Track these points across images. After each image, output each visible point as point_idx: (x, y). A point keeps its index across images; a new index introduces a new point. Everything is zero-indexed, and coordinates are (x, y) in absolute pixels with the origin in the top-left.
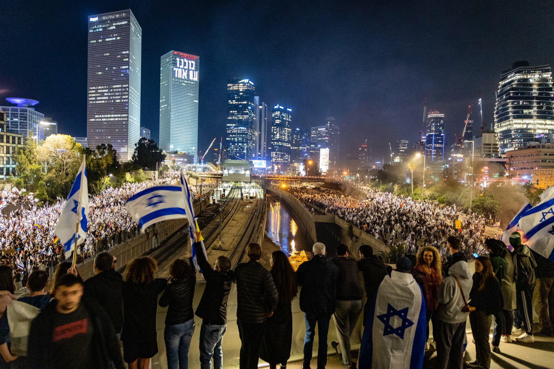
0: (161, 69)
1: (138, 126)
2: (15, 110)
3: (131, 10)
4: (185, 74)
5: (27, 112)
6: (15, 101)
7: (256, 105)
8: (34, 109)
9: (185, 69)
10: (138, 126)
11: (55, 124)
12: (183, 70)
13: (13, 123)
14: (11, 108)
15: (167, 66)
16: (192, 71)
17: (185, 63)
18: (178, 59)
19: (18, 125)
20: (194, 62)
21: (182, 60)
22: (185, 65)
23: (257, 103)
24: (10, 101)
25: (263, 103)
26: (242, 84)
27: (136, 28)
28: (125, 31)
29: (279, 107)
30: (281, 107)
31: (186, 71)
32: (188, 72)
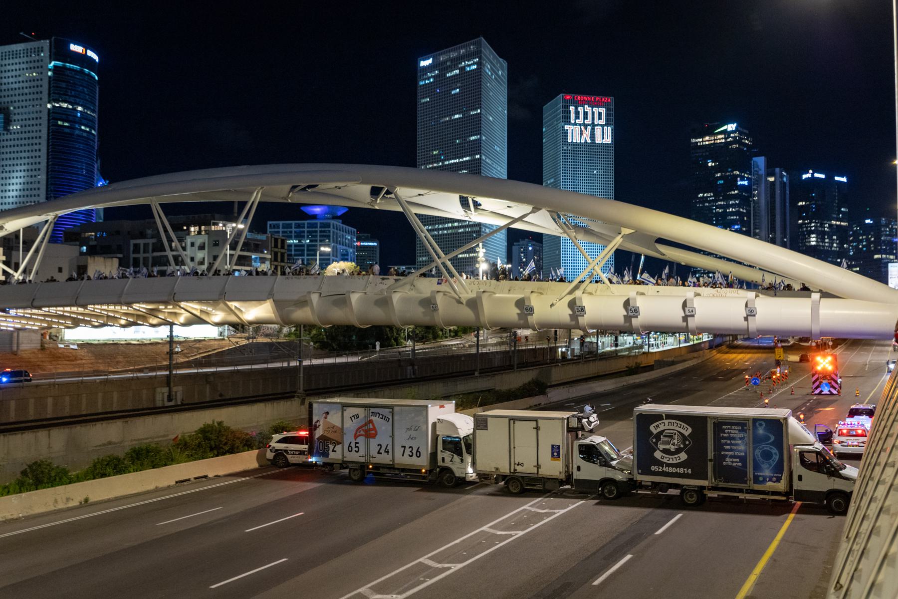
0: (544, 130)
1: (503, 240)
2: (310, 225)
3: (482, 38)
4: (587, 133)
5: (329, 227)
6: (314, 211)
7: (760, 176)
8: (341, 221)
10: (503, 240)
11: (376, 244)
13: (310, 248)
14: (321, 223)
17: (586, 114)
18: (572, 108)
19: (304, 250)
20: (603, 110)
21: (580, 109)
23: (762, 172)
24: (305, 211)
25: (777, 170)
26: (722, 136)
27: (494, 65)
28: (473, 82)
29: (813, 174)
30: (816, 175)
31: (589, 128)
32: (593, 130)
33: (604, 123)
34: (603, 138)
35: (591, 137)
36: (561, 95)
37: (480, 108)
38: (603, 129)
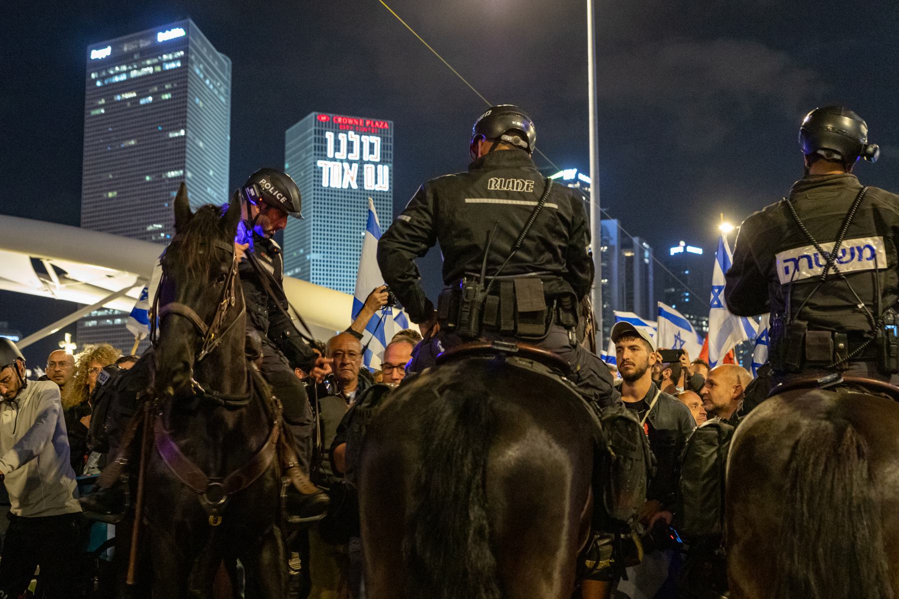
0: (287, 166)
9: (351, 162)
12: (346, 165)
15: (300, 157)
16: (373, 166)
17: (350, 144)
18: (329, 136)
20: (376, 140)
22: (350, 149)
27: (209, 64)
29: (685, 248)
30: (690, 249)
31: (355, 166)
32: (361, 169)
33: (378, 160)
34: (376, 183)
35: (357, 181)
36: (313, 114)
37: (184, 127)
38: (376, 169)
